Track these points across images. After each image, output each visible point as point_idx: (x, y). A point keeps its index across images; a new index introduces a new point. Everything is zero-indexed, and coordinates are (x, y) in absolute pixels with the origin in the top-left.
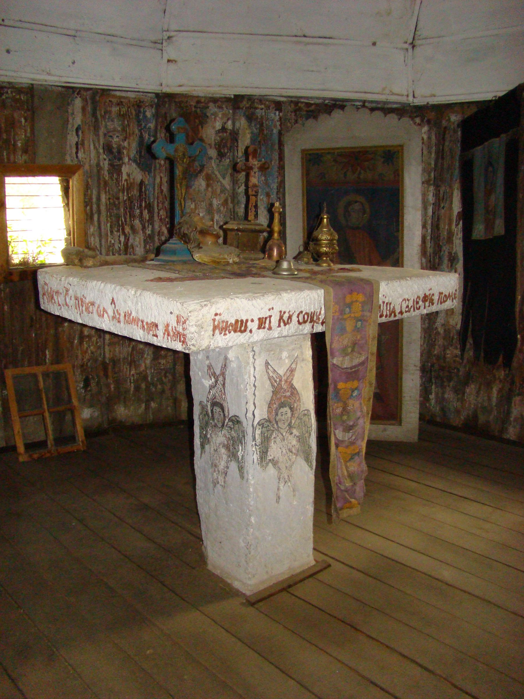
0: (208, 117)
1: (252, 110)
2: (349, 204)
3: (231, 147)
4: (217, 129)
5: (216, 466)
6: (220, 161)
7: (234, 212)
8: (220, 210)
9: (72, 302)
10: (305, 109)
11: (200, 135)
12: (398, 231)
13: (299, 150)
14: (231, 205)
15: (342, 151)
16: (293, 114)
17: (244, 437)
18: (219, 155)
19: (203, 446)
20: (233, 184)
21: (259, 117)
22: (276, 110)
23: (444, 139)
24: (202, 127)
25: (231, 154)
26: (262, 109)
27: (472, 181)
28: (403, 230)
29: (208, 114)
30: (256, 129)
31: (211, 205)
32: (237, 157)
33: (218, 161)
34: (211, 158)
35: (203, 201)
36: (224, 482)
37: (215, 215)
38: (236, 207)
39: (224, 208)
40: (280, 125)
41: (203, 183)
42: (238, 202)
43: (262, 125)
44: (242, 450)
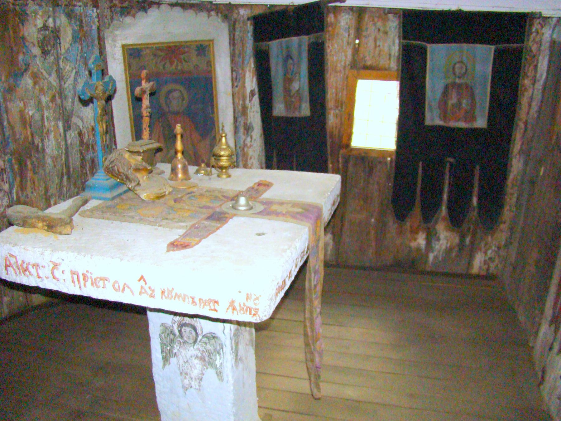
0: (27, 14)
1: (71, 7)
2: (170, 92)
3: (54, 45)
4: (39, 27)
5: (186, 374)
6: (45, 59)
7: (62, 106)
8: (49, 107)
9: (68, 275)
10: (120, 5)
11: (22, 33)
12: (213, 112)
13: (120, 45)
14: (59, 101)
15: (160, 45)
16: (109, 11)
17: (222, 348)
18: (42, 53)
19: (166, 360)
20: (60, 80)
21: (79, 14)
22: (93, 7)
23: (234, 29)
24: (23, 25)
25: (55, 51)
26: (80, 6)
27: (268, 70)
28: (217, 112)
29: (28, 12)
30: (77, 26)
31: (40, 102)
32: (61, 54)
33: (43, 59)
34: (35, 56)
35: (31, 99)
36: (199, 386)
37: (45, 111)
38: (64, 102)
39: (53, 103)
40: (98, 22)
41: (30, 82)
42: (66, 97)
43: (81, 22)
44: (220, 359)
